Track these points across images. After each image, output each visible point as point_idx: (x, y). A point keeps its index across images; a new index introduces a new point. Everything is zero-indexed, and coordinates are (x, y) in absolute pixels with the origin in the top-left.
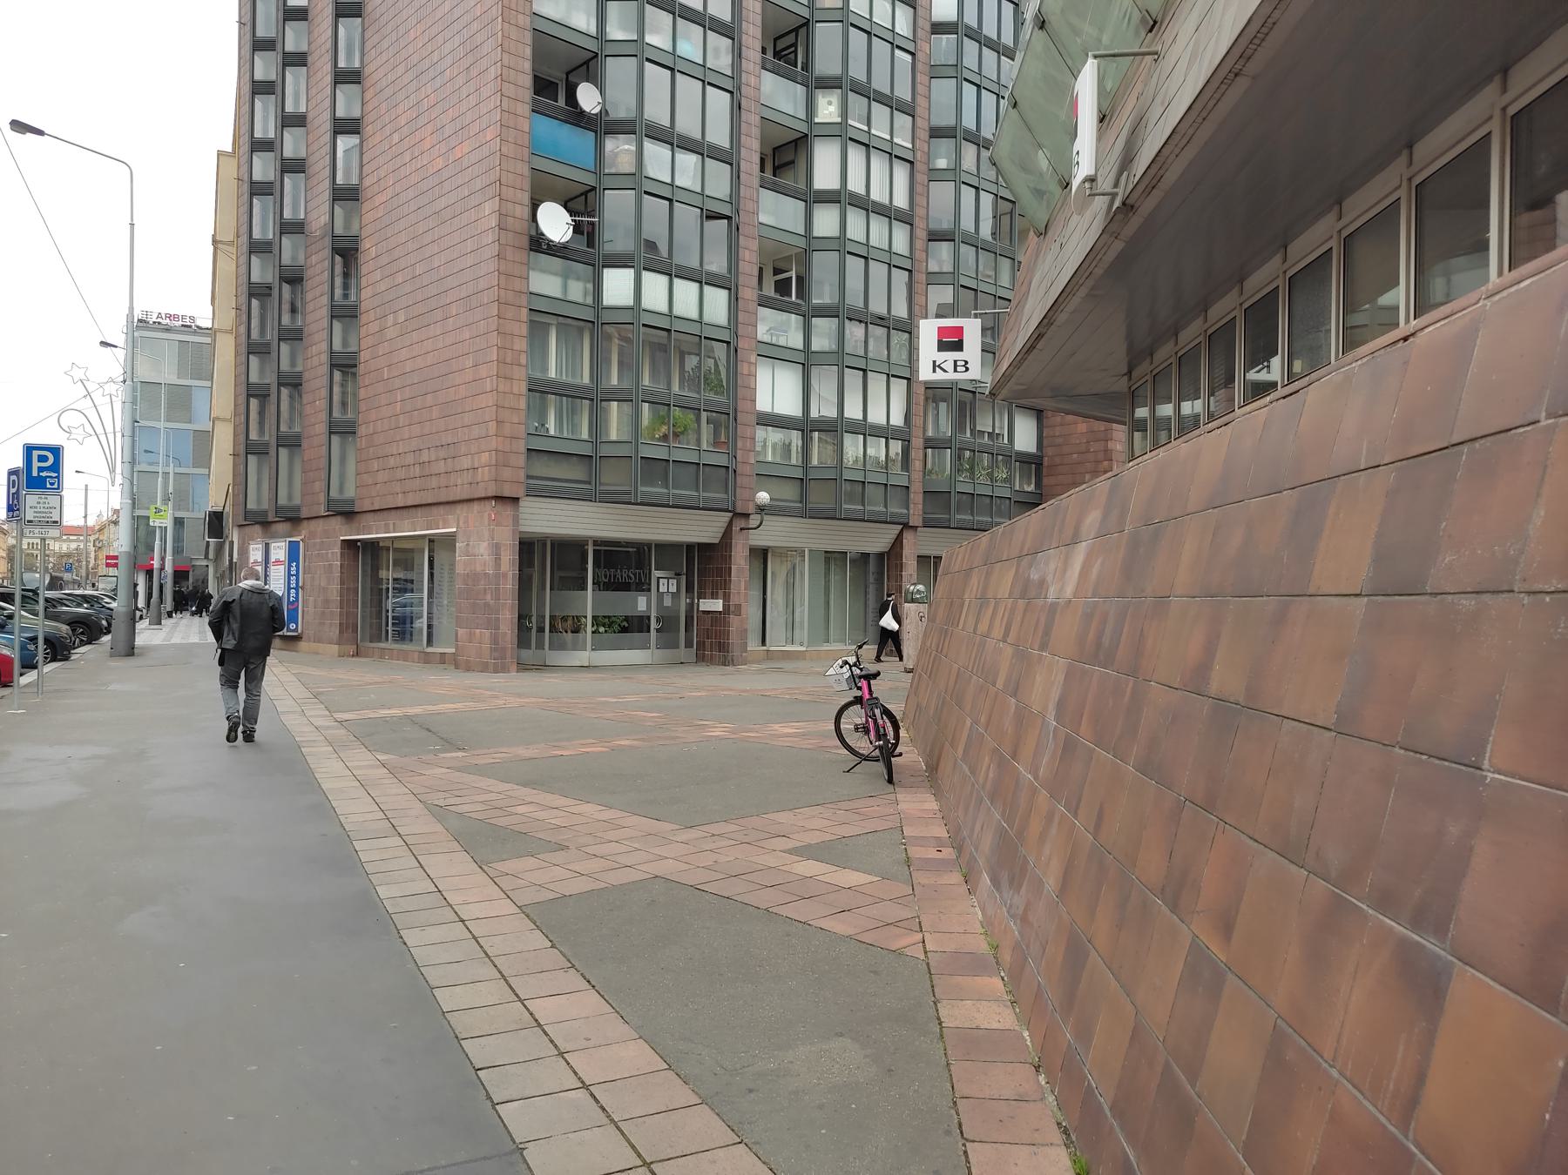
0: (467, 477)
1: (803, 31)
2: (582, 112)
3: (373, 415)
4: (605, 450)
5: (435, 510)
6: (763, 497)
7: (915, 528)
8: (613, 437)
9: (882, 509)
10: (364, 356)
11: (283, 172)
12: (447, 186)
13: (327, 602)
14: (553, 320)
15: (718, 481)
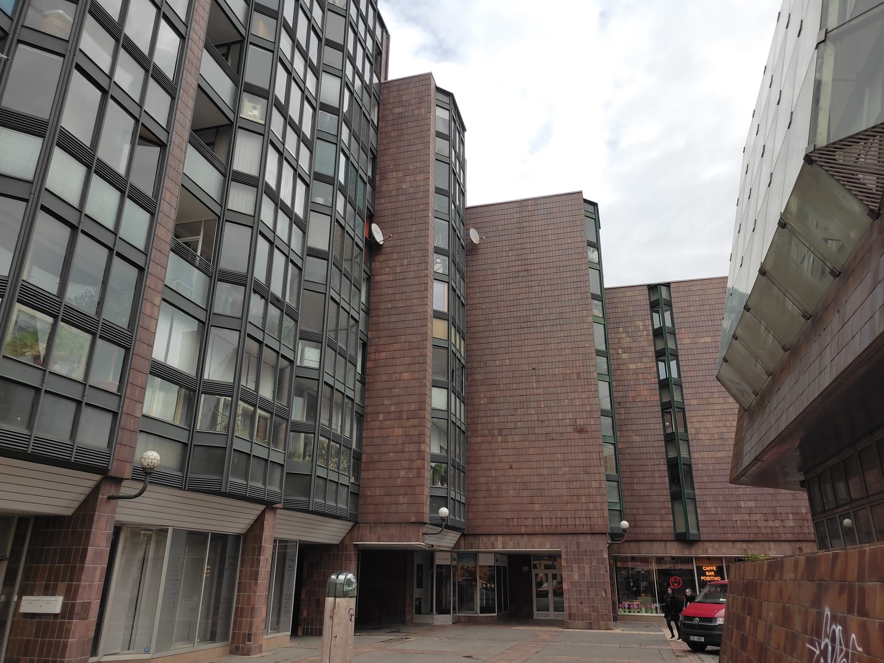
1: (235, 49)
9: (322, 501)
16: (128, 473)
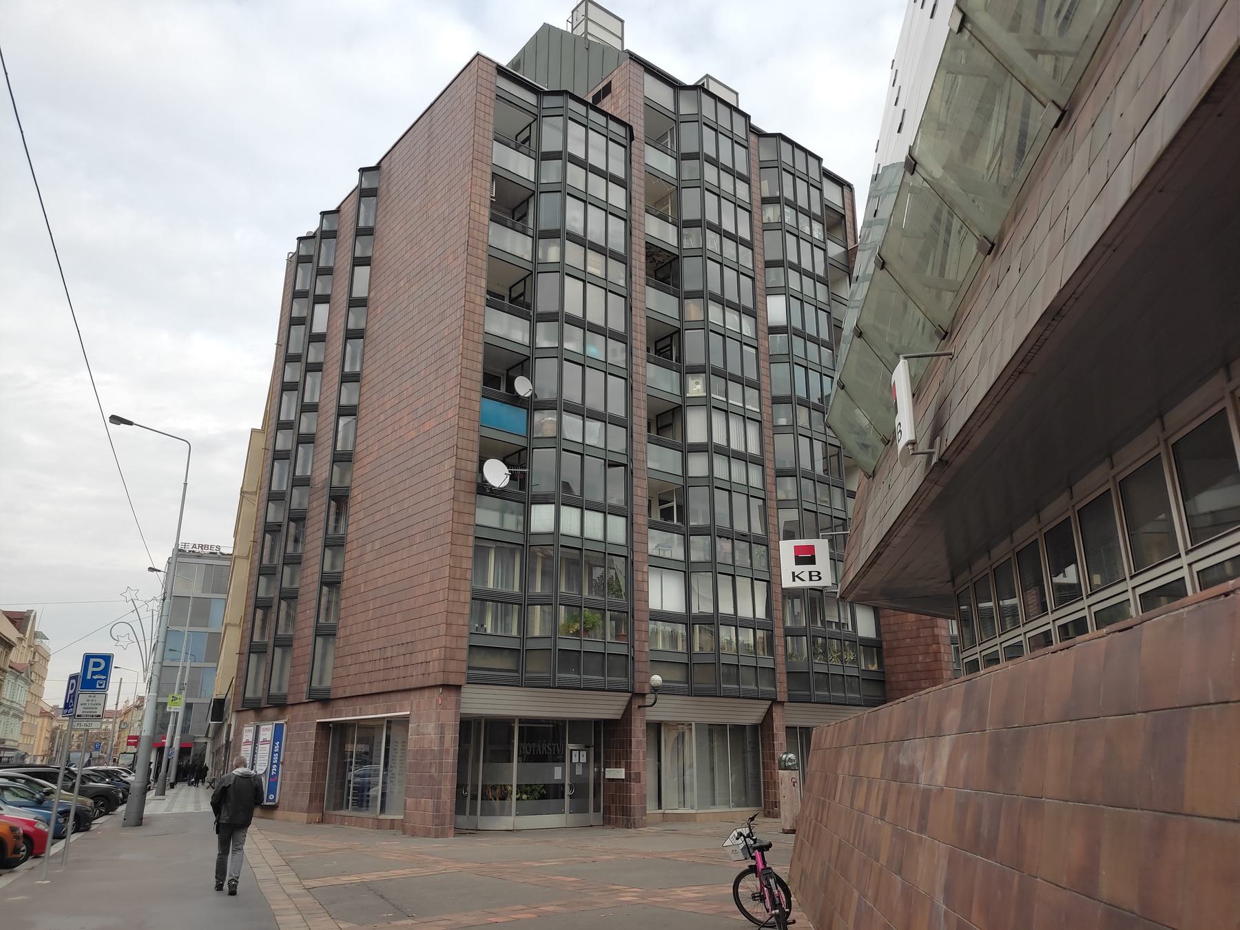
1: (676, 336)
2: (518, 396)
4: (531, 645)
5: (393, 696)
6: (657, 679)
7: (782, 703)
8: (537, 633)
10: (346, 575)
13: (301, 775)
15: (619, 668)
16: (647, 690)
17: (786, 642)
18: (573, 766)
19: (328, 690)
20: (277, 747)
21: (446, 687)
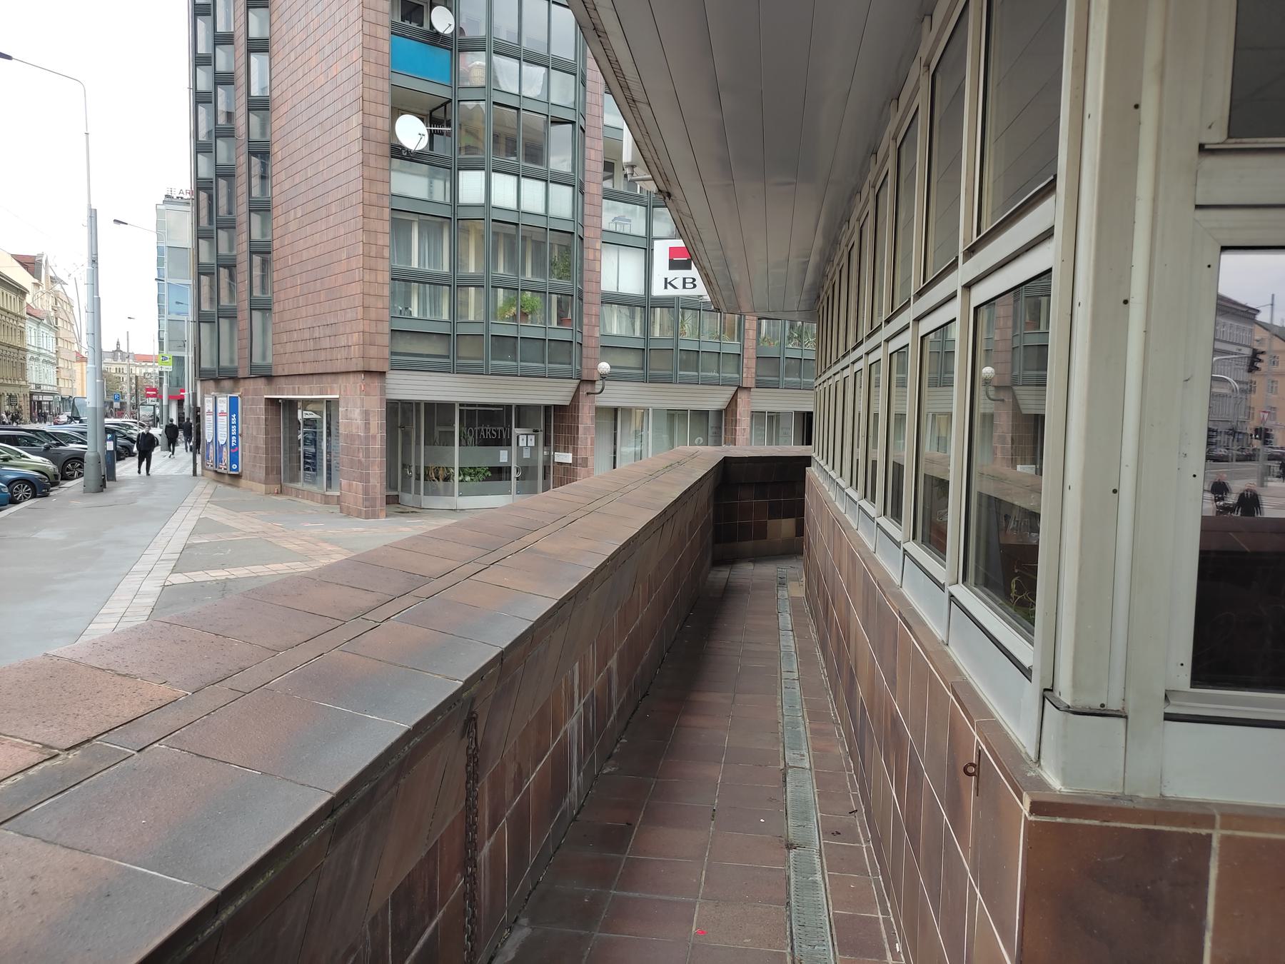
0: (342, 354)
2: (438, 33)
3: (282, 296)
4: (462, 330)
5: (324, 377)
6: (604, 367)
7: (748, 389)
8: (471, 318)
10: (276, 244)
11: (216, 84)
12: (328, 100)
13: (257, 448)
14: (410, 217)
15: (560, 353)
17: (759, 325)
18: (520, 449)
19: (270, 367)
20: (234, 420)
21: (368, 373)
